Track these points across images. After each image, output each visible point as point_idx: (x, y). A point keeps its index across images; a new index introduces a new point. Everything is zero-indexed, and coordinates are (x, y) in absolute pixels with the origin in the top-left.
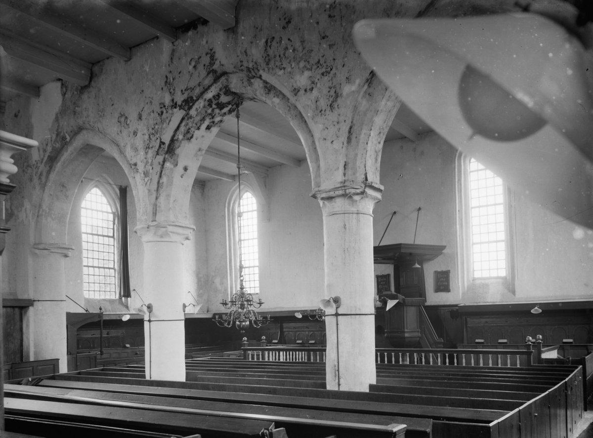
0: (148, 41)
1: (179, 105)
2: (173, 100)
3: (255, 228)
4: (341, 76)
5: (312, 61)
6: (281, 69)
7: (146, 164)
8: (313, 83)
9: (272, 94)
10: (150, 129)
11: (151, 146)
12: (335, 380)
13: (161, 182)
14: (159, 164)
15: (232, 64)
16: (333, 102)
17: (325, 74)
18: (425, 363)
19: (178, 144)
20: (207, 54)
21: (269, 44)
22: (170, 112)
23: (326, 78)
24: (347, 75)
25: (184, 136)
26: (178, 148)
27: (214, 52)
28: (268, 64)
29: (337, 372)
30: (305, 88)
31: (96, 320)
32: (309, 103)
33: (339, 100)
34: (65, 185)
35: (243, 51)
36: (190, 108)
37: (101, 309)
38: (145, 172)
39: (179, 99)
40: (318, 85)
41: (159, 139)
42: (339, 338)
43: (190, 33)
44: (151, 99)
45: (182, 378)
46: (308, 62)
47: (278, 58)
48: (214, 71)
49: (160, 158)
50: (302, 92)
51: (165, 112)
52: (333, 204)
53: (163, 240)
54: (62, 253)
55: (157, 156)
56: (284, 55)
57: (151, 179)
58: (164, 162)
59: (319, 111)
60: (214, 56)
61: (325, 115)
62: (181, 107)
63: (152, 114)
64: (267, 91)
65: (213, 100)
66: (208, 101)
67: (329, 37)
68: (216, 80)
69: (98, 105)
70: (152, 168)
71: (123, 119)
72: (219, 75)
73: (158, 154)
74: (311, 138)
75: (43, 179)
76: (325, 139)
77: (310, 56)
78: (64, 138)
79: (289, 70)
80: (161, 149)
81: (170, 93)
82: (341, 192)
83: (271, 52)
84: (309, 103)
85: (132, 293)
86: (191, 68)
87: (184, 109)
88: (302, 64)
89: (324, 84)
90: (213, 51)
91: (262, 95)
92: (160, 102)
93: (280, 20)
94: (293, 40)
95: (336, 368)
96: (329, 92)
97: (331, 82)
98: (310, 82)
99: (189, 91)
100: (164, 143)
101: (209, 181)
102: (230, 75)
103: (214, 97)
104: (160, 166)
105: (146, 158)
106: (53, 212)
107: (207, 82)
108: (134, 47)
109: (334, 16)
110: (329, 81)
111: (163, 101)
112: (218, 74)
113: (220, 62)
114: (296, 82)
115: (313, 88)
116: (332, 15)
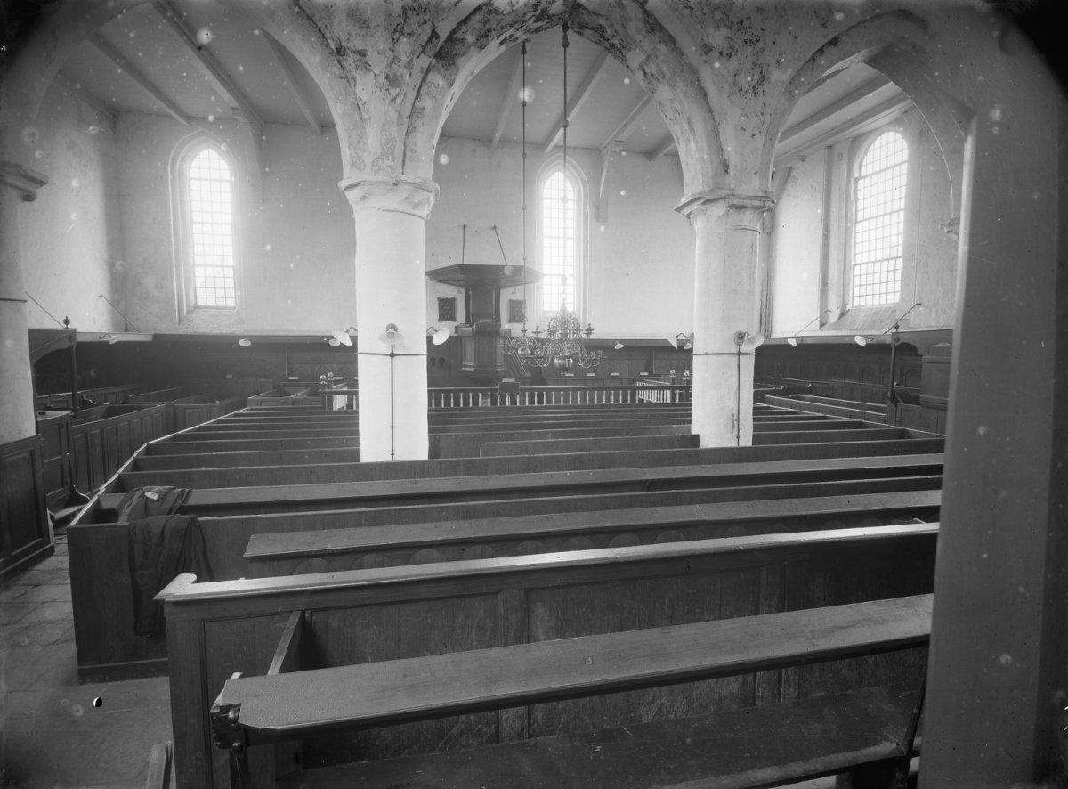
3: (228, 208)
8: (732, 47)
11: (406, 30)
14: (422, 71)
18: (454, 405)
19: (464, 49)
26: (463, 56)
31: (65, 345)
33: (765, 86)
37: (67, 322)
38: (391, 76)
40: (739, 54)
45: (422, 454)
46: (728, 16)
49: (425, 61)
50: (715, 54)
53: (415, 212)
54: (21, 189)
55: (422, 55)
58: (429, 70)
70: (410, 75)
73: (423, 52)
74: (712, 121)
76: (745, 130)
79: (699, 14)
82: (759, 203)
91: (639, 32)
95: (735, 417)
96: (753, 69)
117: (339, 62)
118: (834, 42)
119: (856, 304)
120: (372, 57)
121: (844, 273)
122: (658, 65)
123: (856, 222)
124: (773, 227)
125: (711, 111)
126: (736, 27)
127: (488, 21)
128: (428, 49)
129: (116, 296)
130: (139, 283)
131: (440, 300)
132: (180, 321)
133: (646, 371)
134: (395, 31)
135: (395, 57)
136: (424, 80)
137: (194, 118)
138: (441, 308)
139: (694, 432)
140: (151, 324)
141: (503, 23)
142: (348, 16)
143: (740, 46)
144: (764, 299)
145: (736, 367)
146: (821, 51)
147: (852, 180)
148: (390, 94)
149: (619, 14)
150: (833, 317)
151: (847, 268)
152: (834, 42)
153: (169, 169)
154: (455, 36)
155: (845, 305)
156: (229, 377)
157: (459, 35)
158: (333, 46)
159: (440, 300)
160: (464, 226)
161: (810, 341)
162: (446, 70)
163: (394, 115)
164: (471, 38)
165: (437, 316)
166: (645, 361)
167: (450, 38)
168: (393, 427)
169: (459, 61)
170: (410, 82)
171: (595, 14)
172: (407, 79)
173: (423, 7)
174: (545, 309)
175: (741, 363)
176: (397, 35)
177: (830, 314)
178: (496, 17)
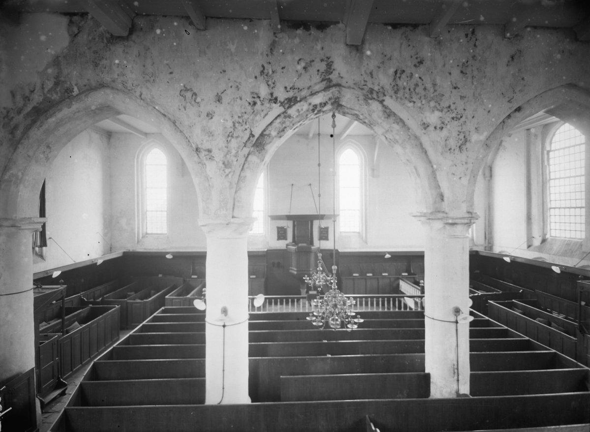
0: (214, 17)
1: (280, 102)
2: (272, 94)
4: (470, 126)
5: (442, 104)
6: (411, 102)
7: (227, 154)
9: (392, 119)
10: (236, 118)
11: (235, 135)
12: (453, 377)
13: (242, 174)
14: (245, 156)
15: (354, 80)
16: (462, 145)
17: (455, 119)
20: (322, 60)
21: (398, 75)
22: (268, 105)
23: (456, 123)
24: (476, 126)
25: (278, 134)
26: (269, 143)
27: (332, 62)
28: (396, 93)
29: (456, 371)
30: (435, 125)
32: (439, 139)
33: (468, 144)
34: (50, 146)
35: (368, 72)
36: (290, 107)
39: (282, 95)
40: (448, 126)
41: (249, 130)
42: (458, 341)
43: (299, 32)
44: (237, 84)
46: (439, 104)
47: (407, 90)
48: (330, 80)
49: (246, 151)
50: (431, 128)
51: (259, 103)
52: (455, 229)
56: (415, 89)
57: (234, 171)
58: (249, 154)
59: (448, 149)
60: (331, 65)
61: (454, 154)
62: (282, 104)
63: (238, 100)
64: (386, 116)
65: (318, 107)
66: (313, 106)
67: (461, 89)
68: (326, 89)
69: (144, 66)
71: (189, 95)
72: (332, 85)
73: (245, 146)
75: (18, 133)
76: (454, 174)
77: (441, 100)
78: (69, 90)
79: (419, 105)
80: (249, 142)
81: (268, 85)
82: (466, 221)
83: (400, 83)
84: (439, 139)
85: (48, 242)
86: (299, 67)
87: (284, 107)
88: (432, 104)
89: (453, 128)
90: (330, 60)
92: (252, 91)
93: (412, 57)
94: (424, 80)
95: (456, 367)
96: (458, 135)
97: (460, 128)
98: (439, 122)
99: (296, 91)
100: (253, 136)
101: (116, 132)
102: (343, 89)
103: (321, 104)
104: (245, 159)
105: (227, 147)
106: (27, 178)
107: (317, 88)
108: (212, 18)
109: (466, 74)
110: (459, 126)
111: (256, 91)
112: (332, 84)
113: (339, 74)
114: (425, 118)
115: (442, 128)
116: (464, 72)
117: (198, 155)
118: (519, 109)
119: (553, 234)
120: (216, 153)
121: (543, 213)
122: (393, 136)
123: (550, 179)
124: (491, 176)
125: (430, 162)
126: (446, 110)
127: (284, 122)
128: (248, 144)
129: (106, 231)
130: (118, 223)
131: (278, 228)
132: (138, 242)
133: (406, 272)
134: (229, 136)
135: (228, 151)
136: (246, 160)
137: (149, 134)
138: (278, 233)
139: (427, 371)
140: (126, 244)
141: (293, 122)
142: (202, 130)
143: (449, 122)
144: (487, 223)
145: (455, 331)
146: (509, 116)
147: (545, 152)
148: (225, 172)
149: (366, 109)
150: (537, 242)
151: (545, 210)
152: (519, 109)
153: (136, 161)
154: (265, 133)
155: (544, 235)
156: (160, 276)
157: (267, 132)
158: (194, 146)
159: (278, 228)
160: (292, 185)
161: (519, 260)
162: (259, 153)
163: (227, 184)
164: (274, 133)
165: (276, 237)
166: (406, 264)
167: (262, 135)
168: (224, 370)
169: (267, 147)
170: (237, 165)
171: (352, 109)
172: (235, 163)
173: (245, 121)
174: (341, 231)
175: (458, 328)
176: (230, 138)
177: (534, 239)
178: (289, 119)
